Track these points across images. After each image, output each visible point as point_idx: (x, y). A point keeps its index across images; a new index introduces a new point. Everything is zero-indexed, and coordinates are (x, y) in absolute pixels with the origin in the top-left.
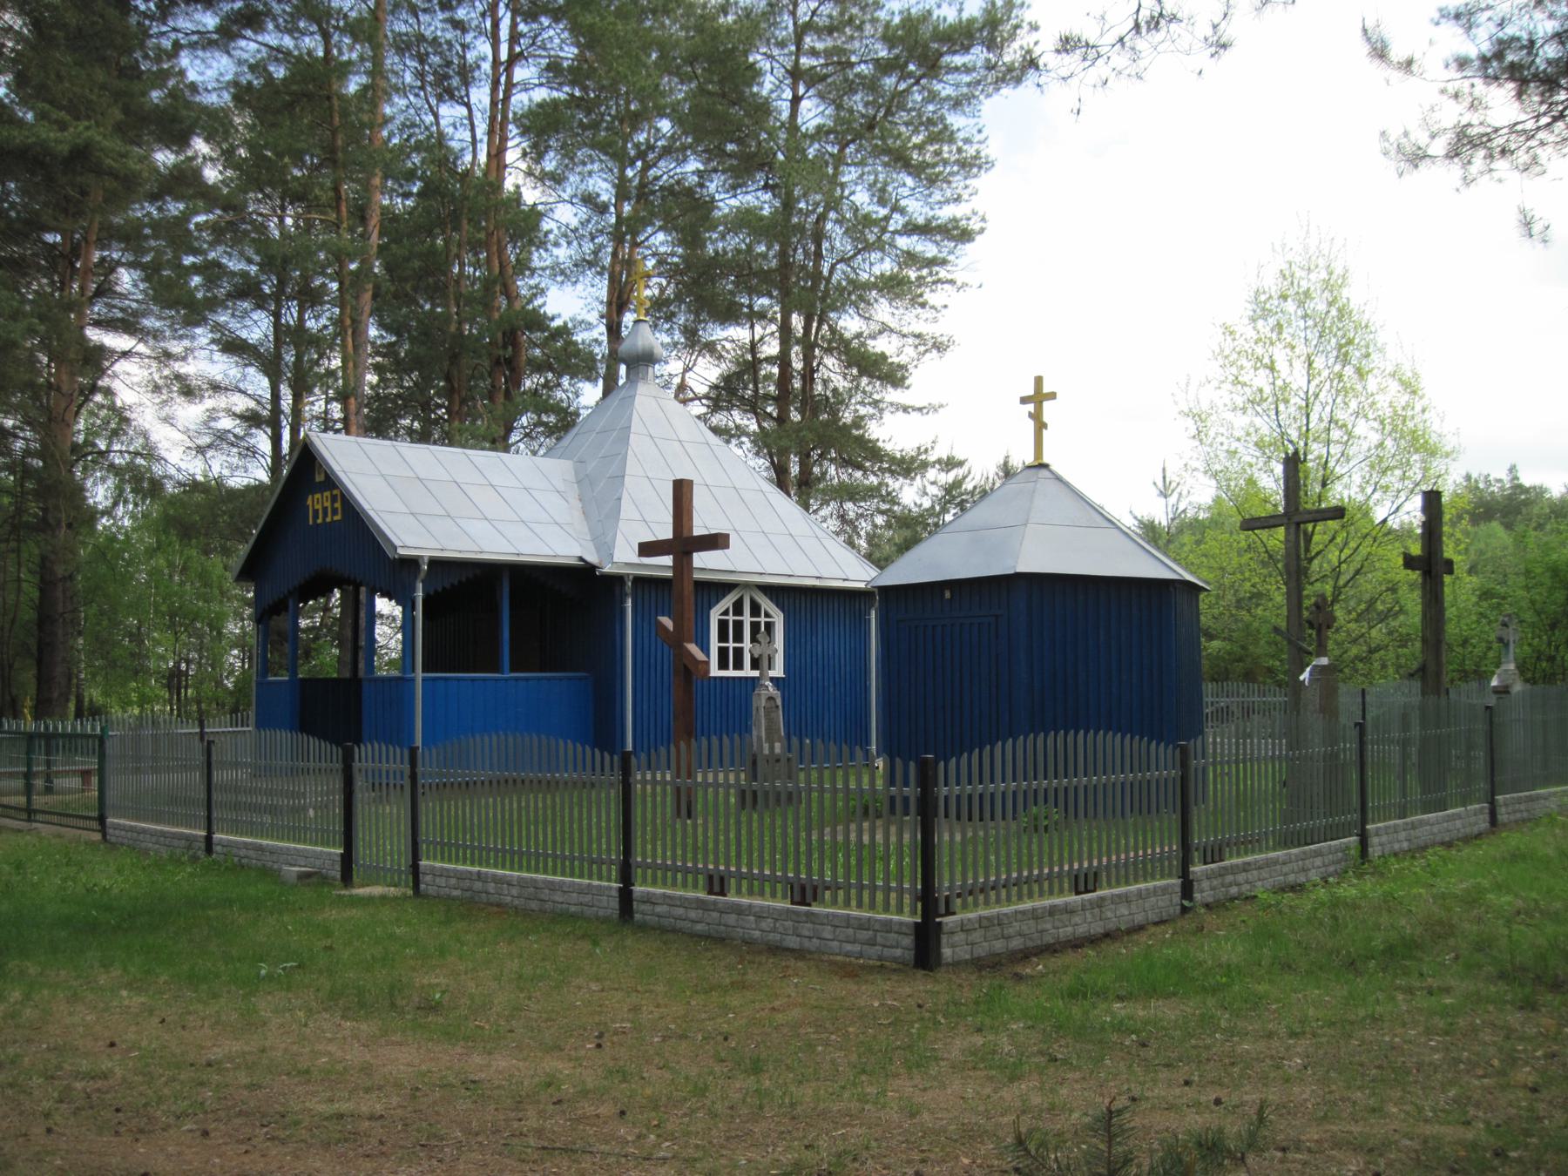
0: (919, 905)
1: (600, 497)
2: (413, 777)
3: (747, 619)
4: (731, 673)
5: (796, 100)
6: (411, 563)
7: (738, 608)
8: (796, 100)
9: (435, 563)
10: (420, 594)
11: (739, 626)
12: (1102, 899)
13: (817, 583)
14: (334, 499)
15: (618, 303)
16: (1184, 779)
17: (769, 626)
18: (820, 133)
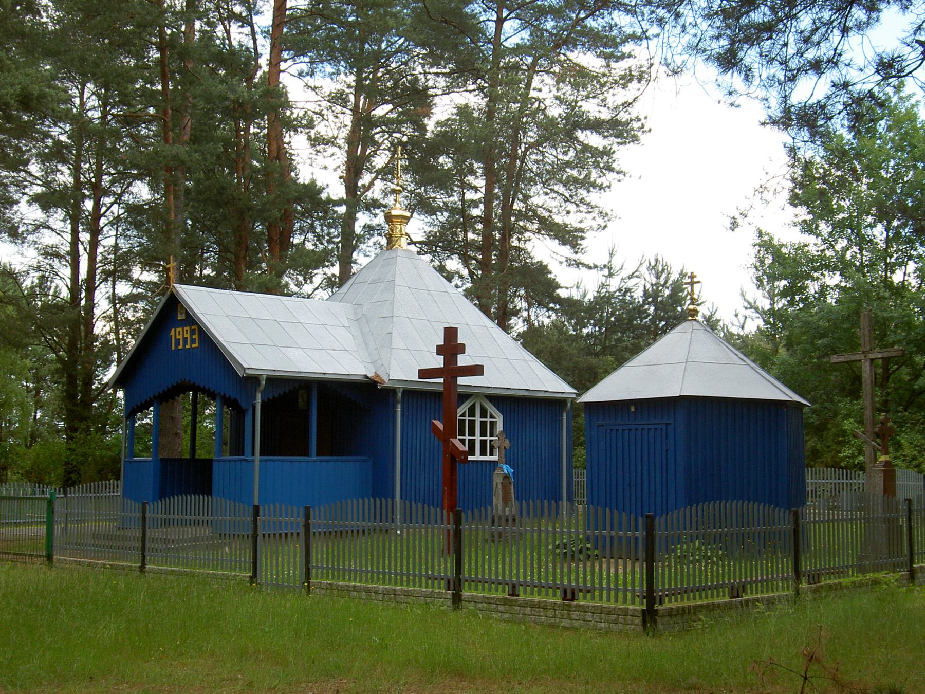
0: (645, 601)
1: (373, 328)
2: (307, 527)
3: (478, 419)
4: (488, 458)
5: (500, 22)
6: (252, 380)
7: (472, 412)
8: (500, 22)
10: (259, 401)
11: (472, 423)
12: (747, 601)
13: (526, 394)
14: (193, 332)
15: (354, 168)
16: (796, 532)
17: (493, 424)
18: (519, 50)
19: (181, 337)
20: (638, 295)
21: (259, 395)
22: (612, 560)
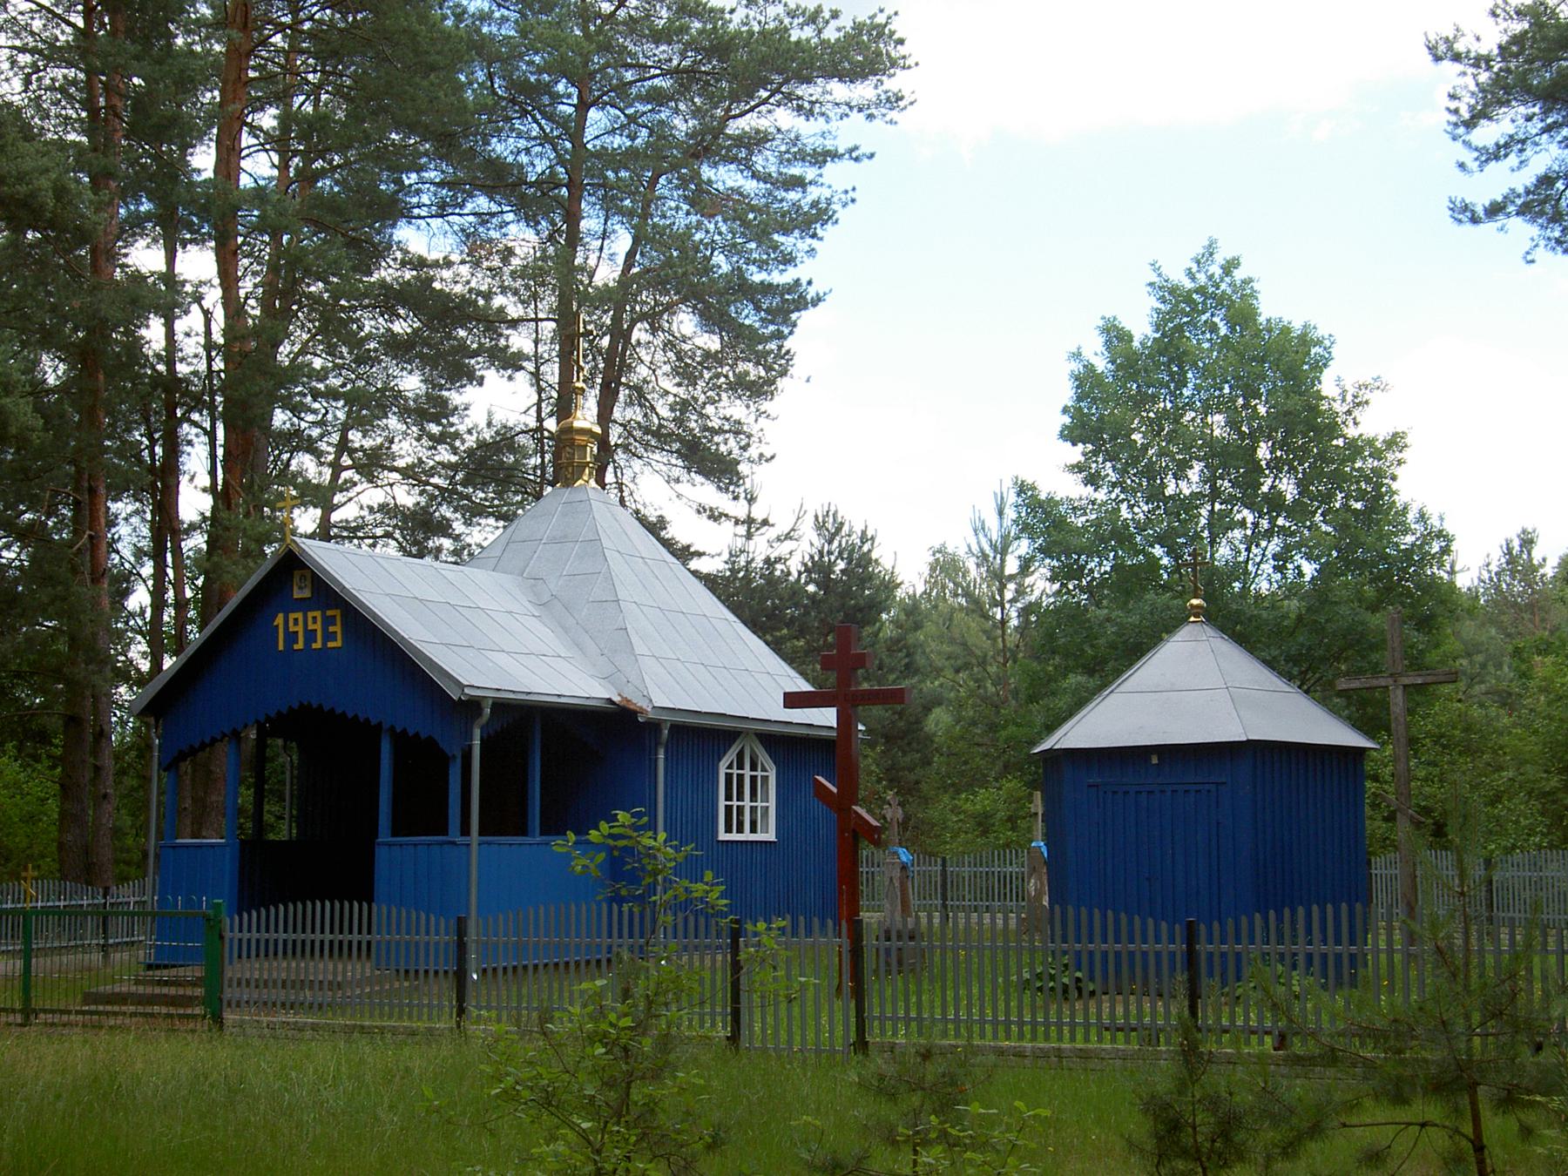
4: (747, 836)
9: (677, 729)
10: (477, 742)
17: (765, 779)
19: (300, 629)
20: (795, 566)
21: (477, 733)
22: (1120, 998)
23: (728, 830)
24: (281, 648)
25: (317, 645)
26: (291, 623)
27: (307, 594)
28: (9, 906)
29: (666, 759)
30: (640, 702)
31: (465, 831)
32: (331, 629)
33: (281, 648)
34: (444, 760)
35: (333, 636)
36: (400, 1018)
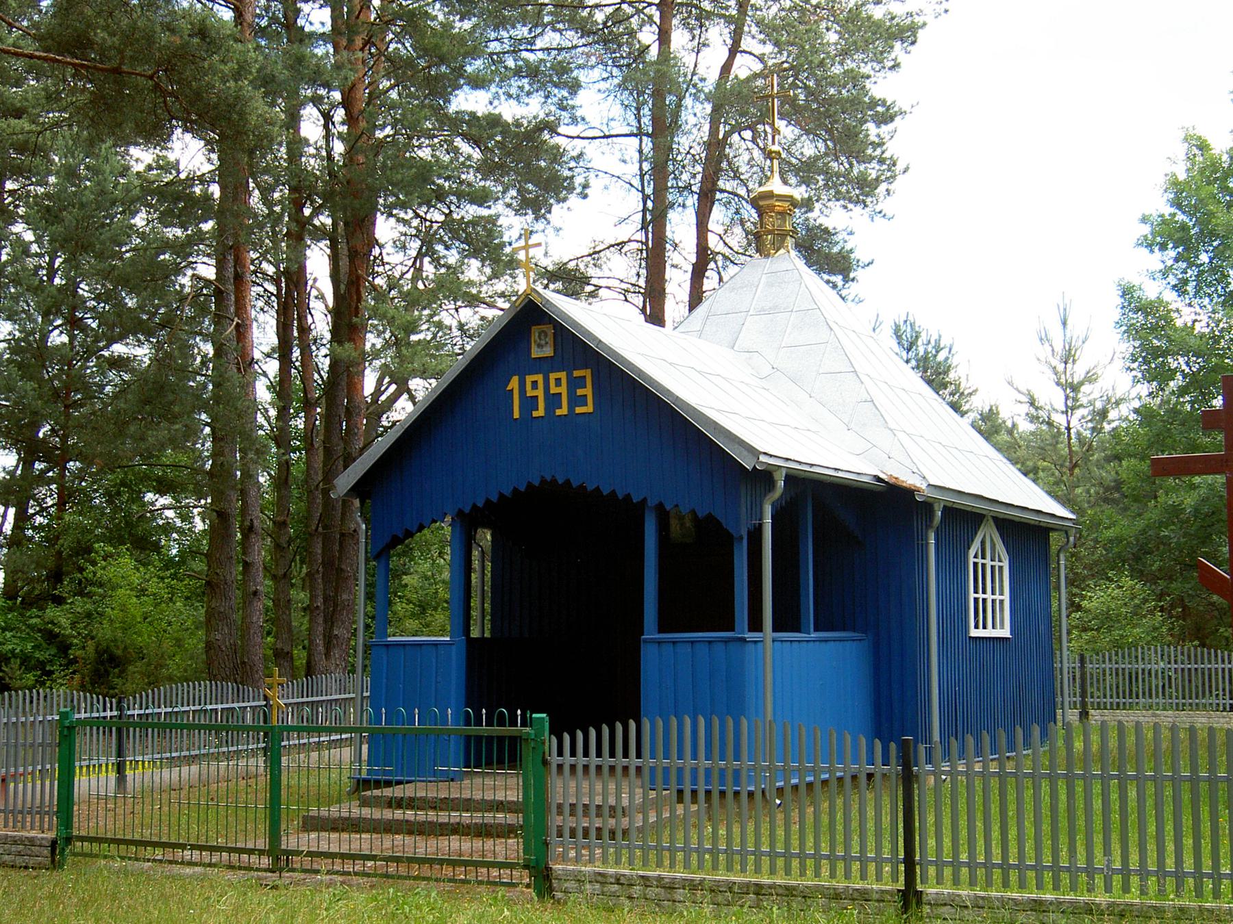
9: (952, 513)
10: (768, 521)
19: (540, 392)
23: (976, 627)
24: (516, 415)
25: (563, 411)
26: (529, 386)
27: (548, 352)
28: (83, 715)
29: (937, 545)
30: (909, 479)
31: (756, 625)
32: (580, 392)
33: (516, 415)
34: (726, 541)
35: (583, 400)
36: (989, 883)
